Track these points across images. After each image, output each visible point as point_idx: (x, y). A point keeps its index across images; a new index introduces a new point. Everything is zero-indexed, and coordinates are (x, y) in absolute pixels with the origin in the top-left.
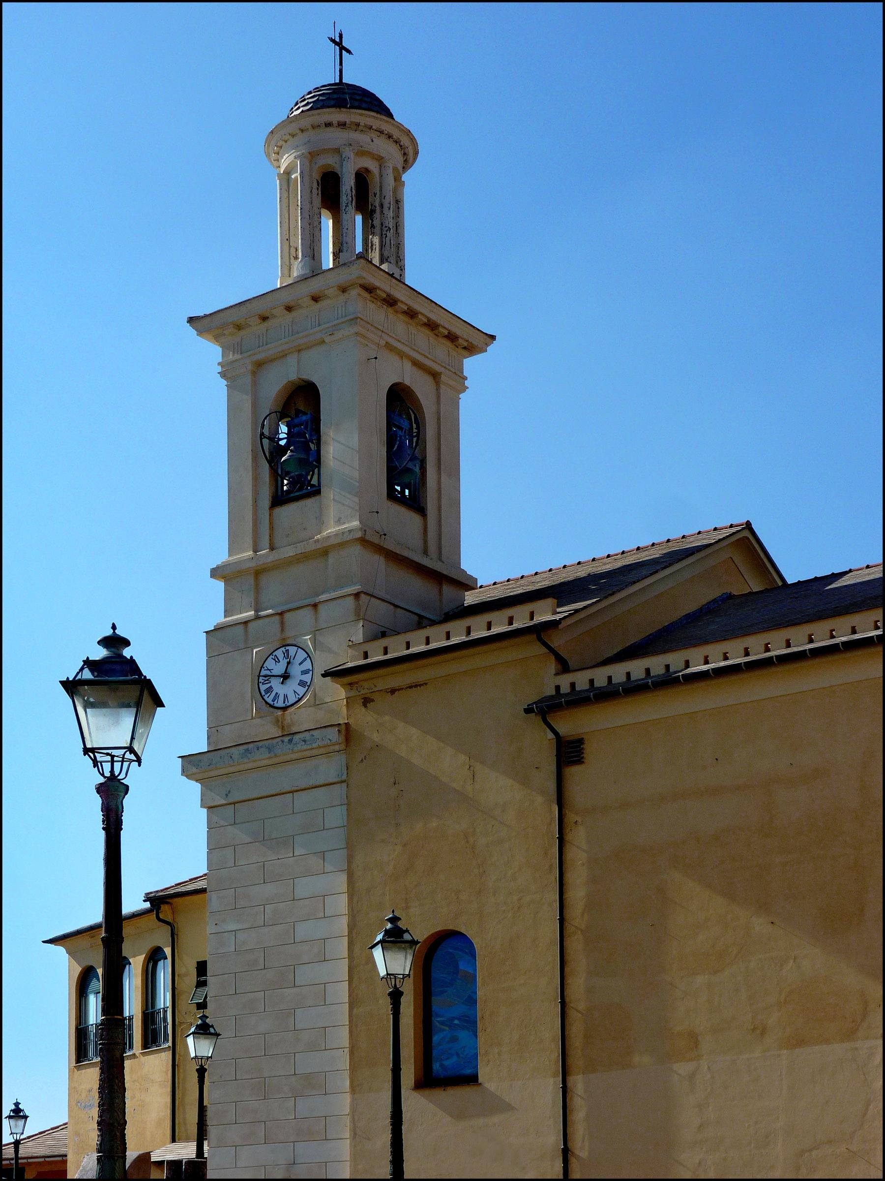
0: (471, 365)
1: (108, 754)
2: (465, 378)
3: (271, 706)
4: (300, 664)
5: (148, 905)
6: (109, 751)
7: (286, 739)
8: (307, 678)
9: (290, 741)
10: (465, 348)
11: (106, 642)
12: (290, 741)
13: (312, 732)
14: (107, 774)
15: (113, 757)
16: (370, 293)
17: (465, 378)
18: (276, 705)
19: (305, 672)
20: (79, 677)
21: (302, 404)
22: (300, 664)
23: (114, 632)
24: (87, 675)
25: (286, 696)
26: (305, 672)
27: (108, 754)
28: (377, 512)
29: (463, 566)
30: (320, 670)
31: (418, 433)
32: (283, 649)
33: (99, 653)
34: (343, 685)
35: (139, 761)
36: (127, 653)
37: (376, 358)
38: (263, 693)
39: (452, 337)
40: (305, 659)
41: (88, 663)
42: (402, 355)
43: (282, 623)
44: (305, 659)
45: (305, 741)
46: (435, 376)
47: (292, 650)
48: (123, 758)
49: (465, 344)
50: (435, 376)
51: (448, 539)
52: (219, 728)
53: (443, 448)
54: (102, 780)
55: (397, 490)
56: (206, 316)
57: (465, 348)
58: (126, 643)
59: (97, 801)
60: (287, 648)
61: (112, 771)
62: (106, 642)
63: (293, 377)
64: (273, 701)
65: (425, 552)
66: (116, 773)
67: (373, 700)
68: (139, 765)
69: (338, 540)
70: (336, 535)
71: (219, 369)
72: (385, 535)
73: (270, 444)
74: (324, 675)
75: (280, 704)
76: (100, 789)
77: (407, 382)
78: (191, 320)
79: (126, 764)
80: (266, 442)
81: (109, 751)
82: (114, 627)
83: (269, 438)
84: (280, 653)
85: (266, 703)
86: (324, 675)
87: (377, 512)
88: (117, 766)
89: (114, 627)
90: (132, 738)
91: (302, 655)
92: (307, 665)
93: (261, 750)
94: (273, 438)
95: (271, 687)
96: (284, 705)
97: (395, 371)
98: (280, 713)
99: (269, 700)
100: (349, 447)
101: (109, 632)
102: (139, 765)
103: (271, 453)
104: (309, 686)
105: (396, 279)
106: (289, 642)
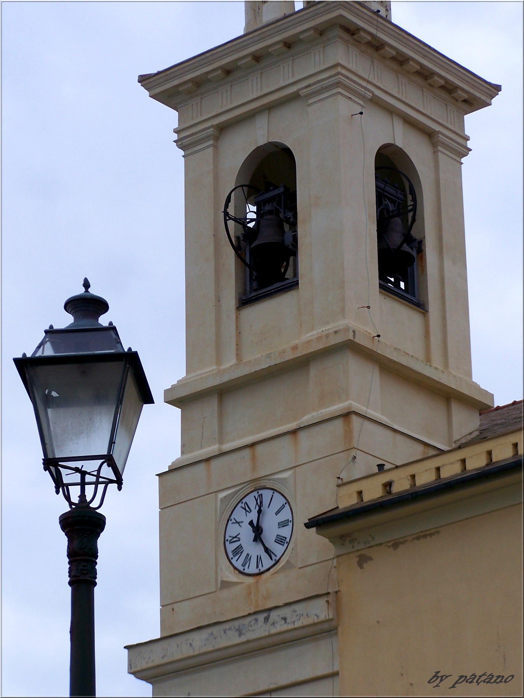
0: (474, 122)
1: (77, 470)
2: (467, 139)
3: (241, 572)
4: (277, 513)
5: (126, 350)
6: (78, 464)
7: (261, 617)
8: (285, 532)
9: (266, 619)
10: (465, 101)
11: (73, 305)
12: (266, 619)
13: (294, 607)
14: (75, 499)
15: (83, 474)
16: (353, 34)
17: (467, 139)
18: (247, 571)
19: (283, 524)
20: (39, 354)
21: (271, 179)
22: (277, 513)
23: (87, 291)
24: (48, 351)
25: (259, 559)
26: (283, 524)
27: (77, 470)
28: (369, 307)
29: (476, 378)
30: (302, 518)
31: (415, 206)
32: (255, 494)
33: (65, 320)
34: (332, 539)
35: (119, 482)
36: (104, 320)
37: (361, 113)
38: (231, 555)
39: (449, 89)
40: (283, 506)
41: (51, 333)
42: (391, 111)
43: (254, 458)
44: (283, 506)
45: (285, 619)
46: (430, 135)
47: (267, 495)
48: (98, 476)
49: (466, 96)
50: (430, 135)
51: (456, 342)
52: (175, 606)
53: (445, 224)
54: (66, 508)
55: (390, 282)
56: (159, 73)
57: (465, 101)
58: (100, 306)
59: (61, 541)
60: (261, 492)
61: (83, 495)
62: (73, 305)
63: (262, 142)
64: (244, 565)
65: (428, 360)
66: (88, 499)
67: (370, 559)
68: (120, 489)
69: (320, 346)
70: (319, 339)
71: (175, 137)
72: (379, 336)
73: (248, 190)
74: (308, 526)
75: (252, 569)
76: (66, 522)
77: (399, 143)
78: (144, 80)
79: (101, 487)
80: (231, 224)
81: (78, 464)
82: (87, 285)
83: (235, 220)
84: (251, 501)
85: (235, 568)
86: (308, 526)
87: (369, 307)
88: (89, 490)
89: (87, 285)
90: (112, 442)
91: (279, 501)
92: (285, 515)
93: (229, 633)
94: (242, 221)
95: (240, 547)
96: (257, 571)
97: (383, 131)
98: (250, 580)
99: (238, 564)
100: (337, 225)
101: (81, 290)
102: (120, 489)
103: (238, 238)
104: (288, 543)
105: (381, 17)
106: (262, 483)
